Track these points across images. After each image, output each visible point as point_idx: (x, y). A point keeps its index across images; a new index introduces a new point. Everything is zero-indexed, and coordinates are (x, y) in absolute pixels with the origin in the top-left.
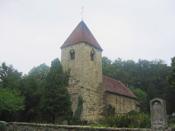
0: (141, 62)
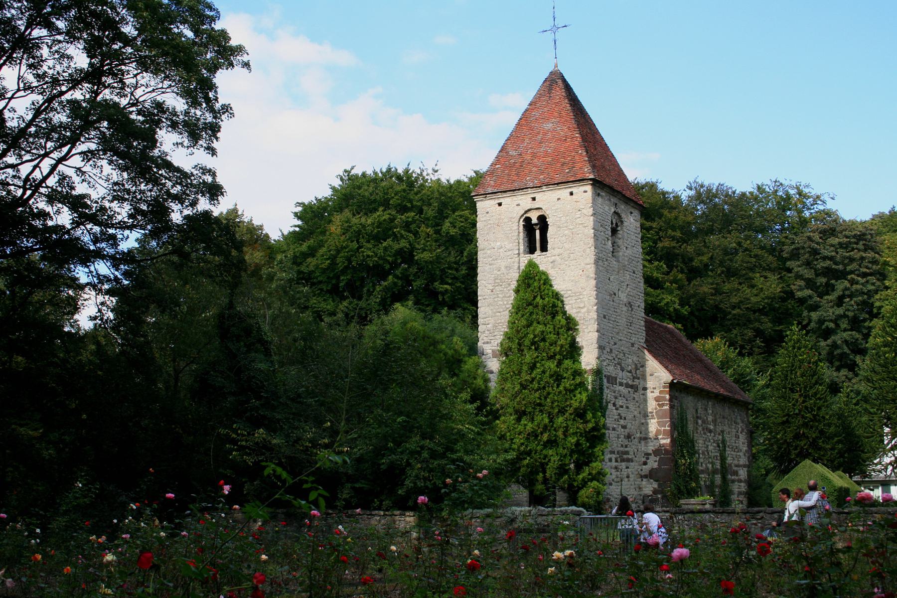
0: (704, 195)
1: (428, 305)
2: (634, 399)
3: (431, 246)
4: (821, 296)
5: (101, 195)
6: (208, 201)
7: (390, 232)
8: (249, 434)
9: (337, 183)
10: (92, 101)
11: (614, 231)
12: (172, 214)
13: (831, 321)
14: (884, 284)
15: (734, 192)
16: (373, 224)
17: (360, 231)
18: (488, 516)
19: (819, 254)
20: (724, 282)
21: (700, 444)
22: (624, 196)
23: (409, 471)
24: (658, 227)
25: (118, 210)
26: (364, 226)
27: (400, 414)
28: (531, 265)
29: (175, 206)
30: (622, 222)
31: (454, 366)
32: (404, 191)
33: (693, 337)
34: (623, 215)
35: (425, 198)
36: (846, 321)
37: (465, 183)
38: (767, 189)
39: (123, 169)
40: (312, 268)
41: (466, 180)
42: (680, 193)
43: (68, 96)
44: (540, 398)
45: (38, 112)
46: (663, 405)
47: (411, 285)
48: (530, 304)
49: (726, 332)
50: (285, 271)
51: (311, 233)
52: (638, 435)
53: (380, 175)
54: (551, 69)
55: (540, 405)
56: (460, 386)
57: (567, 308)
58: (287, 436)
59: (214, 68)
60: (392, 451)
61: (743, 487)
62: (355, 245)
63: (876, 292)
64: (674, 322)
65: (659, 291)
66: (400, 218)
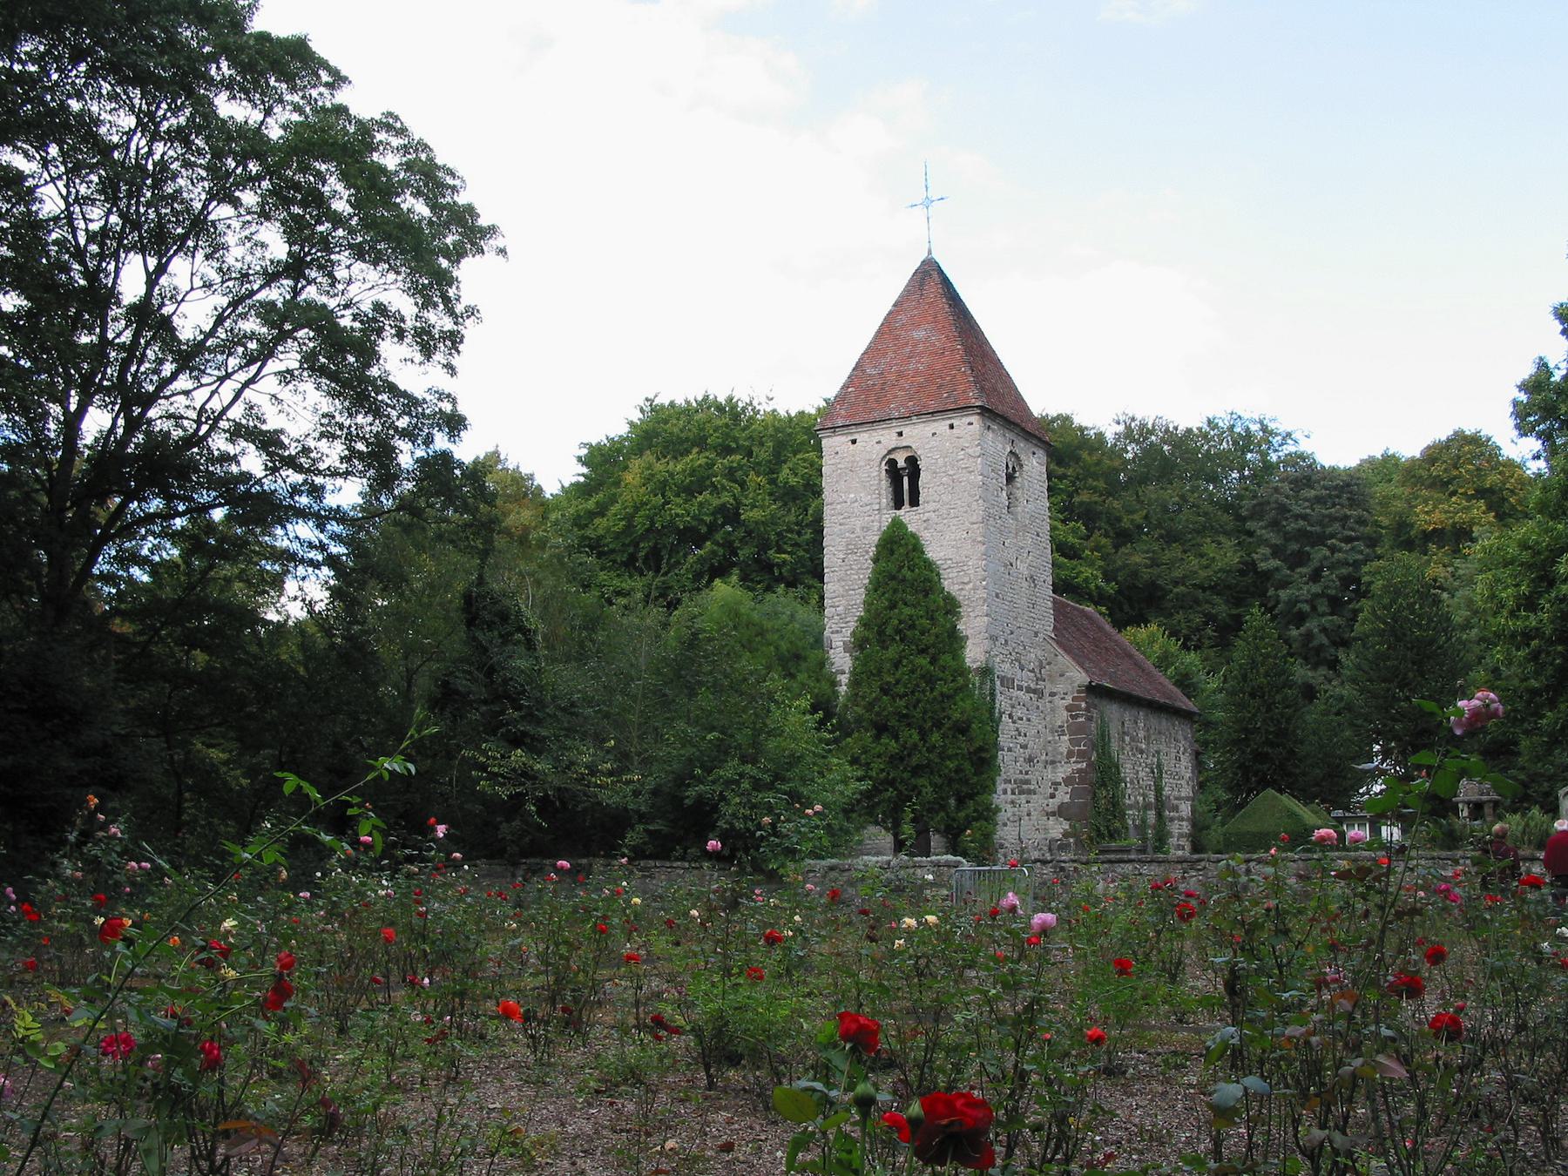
0: (1136, 432)
1: (759, 583)
2: (1038, 708)
3: (763, 500)
4: (1292, 568)
5: (304, 431)
6: (446, 438)
7: (708, 483)
8: (503, 756)
9: (636, 416)
10: (291, 304)
11: (1010, 478)
12: (400, 456)
13: (1306, 601)
14: (1374, 552)
15: (1176, 428)
16: (684, 471)
17: (666, 481)
18: (832, 868)
19: (1289, 511)
20: (1163, 549)
21: (1127, 771)
22: (1023, 430)
23: (723, 807)
24: (1074, 474)
25: (326, 451)
26: (671, 475)
27: (713, 729)
28: (897, 524)
29: (403, 445)
30: (1021, 466)
31: (790, 664)
32: (727, 425)
33: (1120, 625)
34: (1022, 457)
35: (755, 434)
36: (1324, 601)
37: (810, 415)
38: (1221, 424)
39: (332, 394)
40: (601, 532)
41: (813, 411)
42: (1103, 430)
43: (261, 296)
44: (906, 707)
45: (220, 320)
46: (1077, 716)
47: (736, 555)
48: (893, 578)
49: (1166, 618)
50: (561, 535)
51: (601, 485)
52: (1043, 757)
53: (694, 404)
54: (924, 256)
55: (906, 716)
56: (797, 691)
57: (945, 583)
58: (557, 759)
59: (457, 255)
60: (700, 781)
61: (1186, 827)
62: (659, 500)
63: (1365, 562)
64: (1096, 604)
65: (1075, 562)
66: (722, 463)
